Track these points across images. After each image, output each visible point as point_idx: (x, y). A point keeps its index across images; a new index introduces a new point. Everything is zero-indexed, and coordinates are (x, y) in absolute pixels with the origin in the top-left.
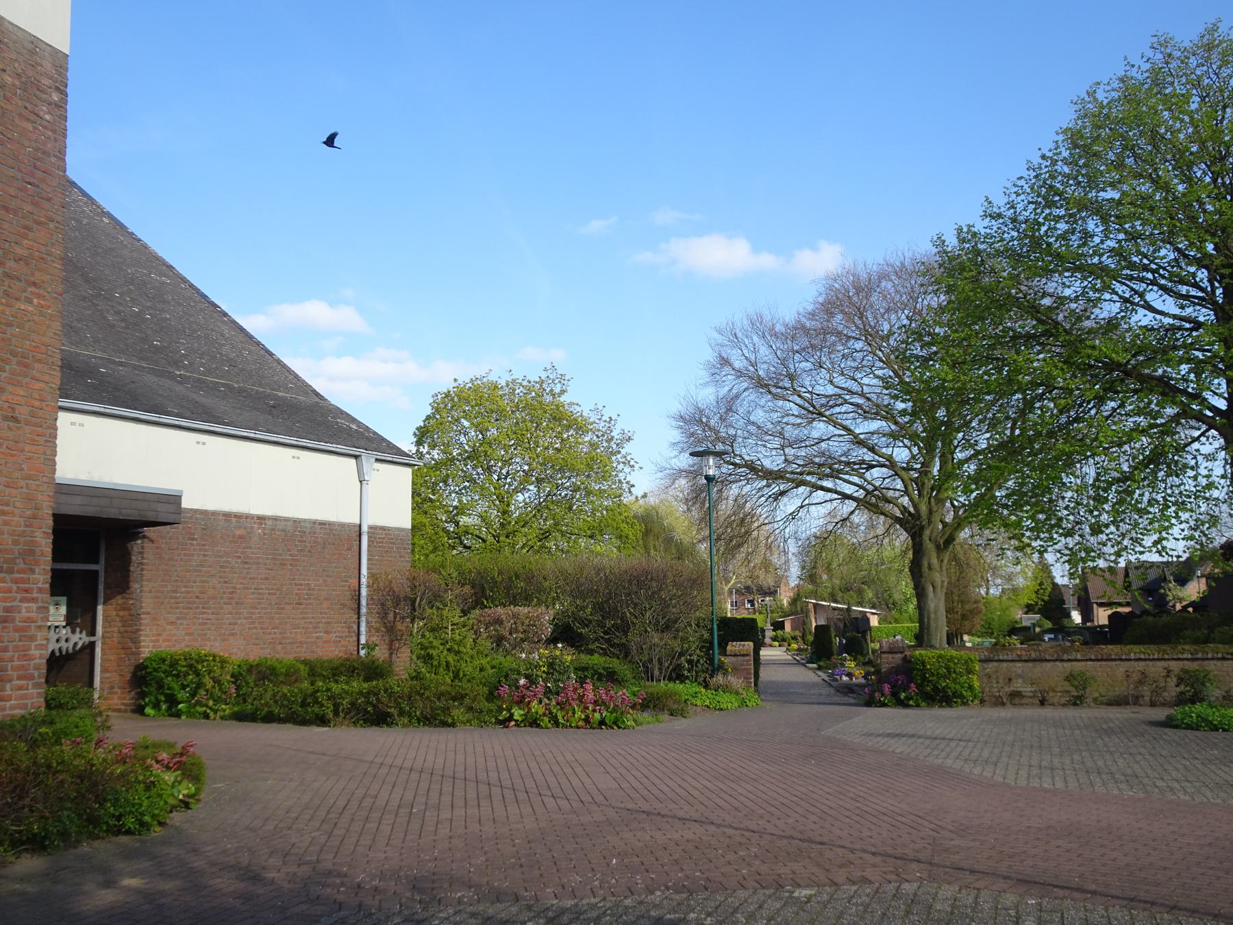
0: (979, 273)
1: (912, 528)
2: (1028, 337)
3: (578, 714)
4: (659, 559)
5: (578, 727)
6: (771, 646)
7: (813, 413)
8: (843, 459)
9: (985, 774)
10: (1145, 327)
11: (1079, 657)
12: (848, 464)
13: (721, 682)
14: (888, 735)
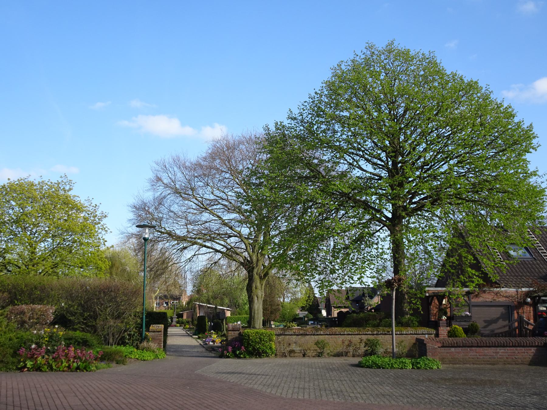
0: (285, 145)
1: (248, 268)
2: (307, 178)
3: (65, 364)
4: (117, 280)
5: (63, 371)
6: (175, 326)
7: (203, 208)
8: (217, 232)
9: (272, 392)
10: (359, 176)
11: (322, 333)
12: (219, 234)
13: (145, 346)
14: (228, 373)
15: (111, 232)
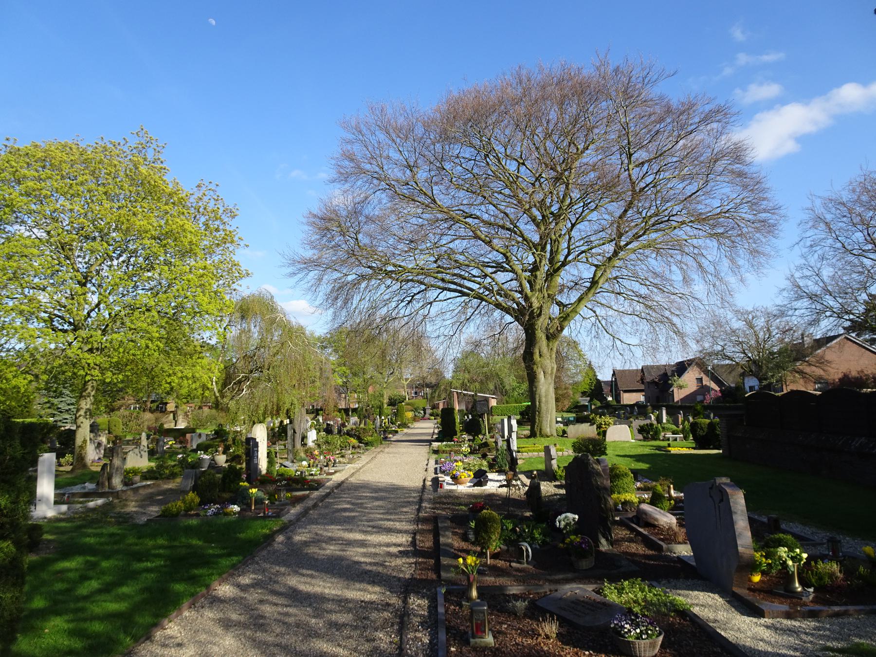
15: (247, 246)
